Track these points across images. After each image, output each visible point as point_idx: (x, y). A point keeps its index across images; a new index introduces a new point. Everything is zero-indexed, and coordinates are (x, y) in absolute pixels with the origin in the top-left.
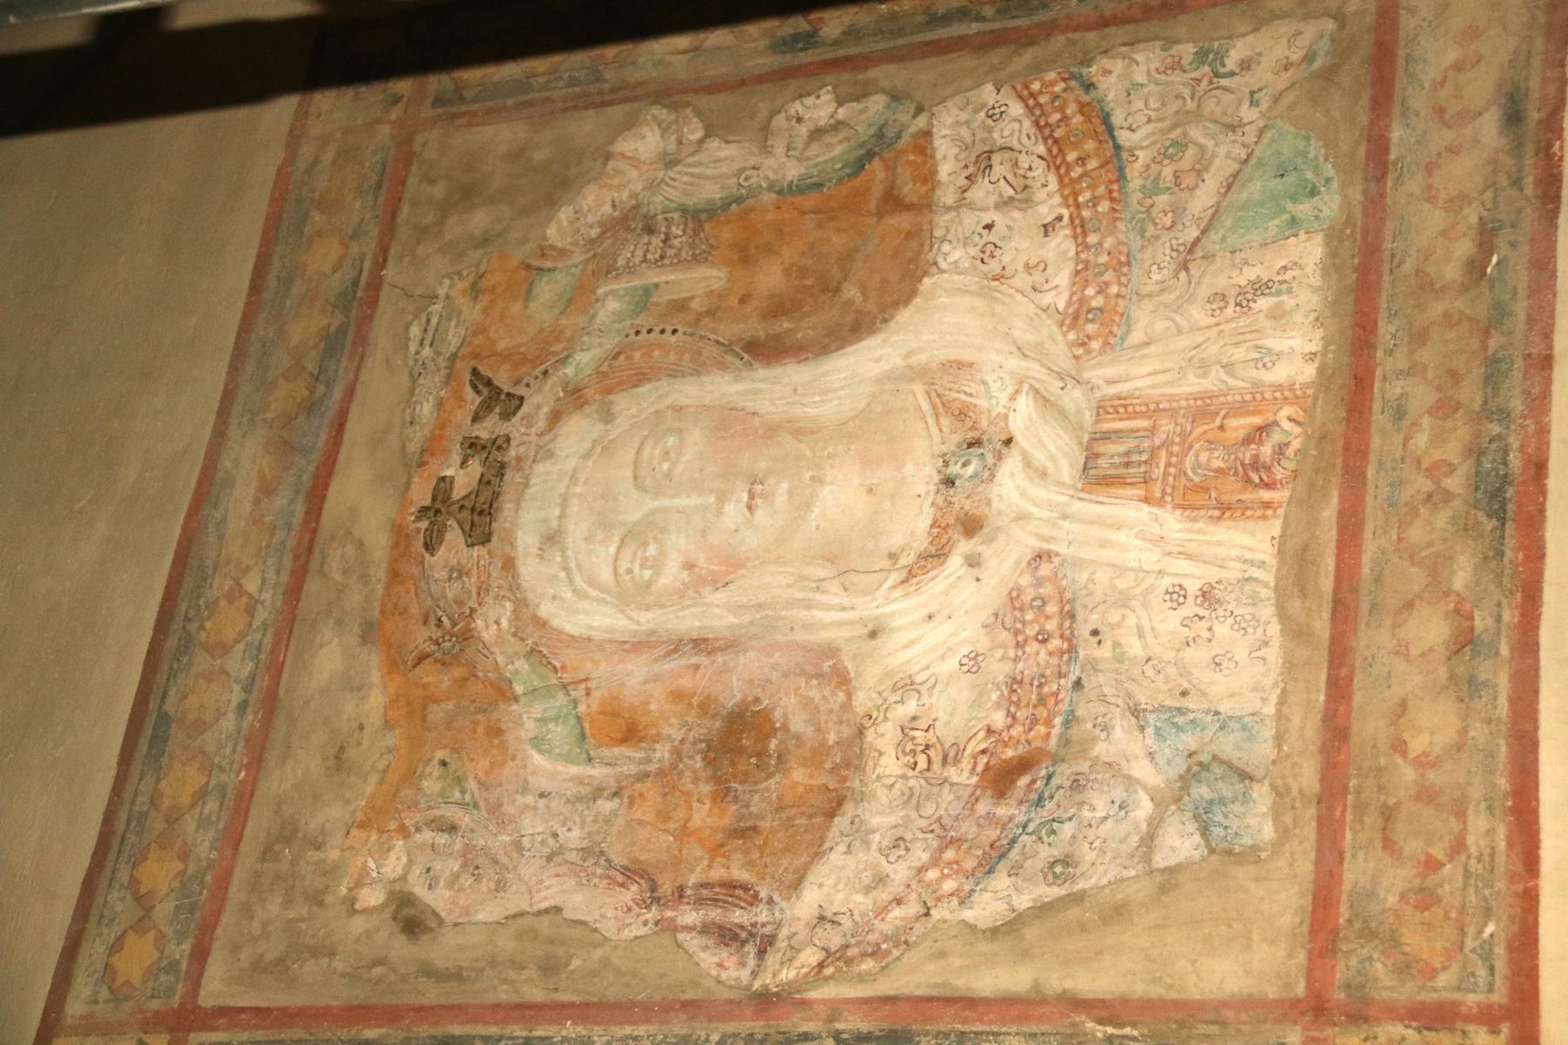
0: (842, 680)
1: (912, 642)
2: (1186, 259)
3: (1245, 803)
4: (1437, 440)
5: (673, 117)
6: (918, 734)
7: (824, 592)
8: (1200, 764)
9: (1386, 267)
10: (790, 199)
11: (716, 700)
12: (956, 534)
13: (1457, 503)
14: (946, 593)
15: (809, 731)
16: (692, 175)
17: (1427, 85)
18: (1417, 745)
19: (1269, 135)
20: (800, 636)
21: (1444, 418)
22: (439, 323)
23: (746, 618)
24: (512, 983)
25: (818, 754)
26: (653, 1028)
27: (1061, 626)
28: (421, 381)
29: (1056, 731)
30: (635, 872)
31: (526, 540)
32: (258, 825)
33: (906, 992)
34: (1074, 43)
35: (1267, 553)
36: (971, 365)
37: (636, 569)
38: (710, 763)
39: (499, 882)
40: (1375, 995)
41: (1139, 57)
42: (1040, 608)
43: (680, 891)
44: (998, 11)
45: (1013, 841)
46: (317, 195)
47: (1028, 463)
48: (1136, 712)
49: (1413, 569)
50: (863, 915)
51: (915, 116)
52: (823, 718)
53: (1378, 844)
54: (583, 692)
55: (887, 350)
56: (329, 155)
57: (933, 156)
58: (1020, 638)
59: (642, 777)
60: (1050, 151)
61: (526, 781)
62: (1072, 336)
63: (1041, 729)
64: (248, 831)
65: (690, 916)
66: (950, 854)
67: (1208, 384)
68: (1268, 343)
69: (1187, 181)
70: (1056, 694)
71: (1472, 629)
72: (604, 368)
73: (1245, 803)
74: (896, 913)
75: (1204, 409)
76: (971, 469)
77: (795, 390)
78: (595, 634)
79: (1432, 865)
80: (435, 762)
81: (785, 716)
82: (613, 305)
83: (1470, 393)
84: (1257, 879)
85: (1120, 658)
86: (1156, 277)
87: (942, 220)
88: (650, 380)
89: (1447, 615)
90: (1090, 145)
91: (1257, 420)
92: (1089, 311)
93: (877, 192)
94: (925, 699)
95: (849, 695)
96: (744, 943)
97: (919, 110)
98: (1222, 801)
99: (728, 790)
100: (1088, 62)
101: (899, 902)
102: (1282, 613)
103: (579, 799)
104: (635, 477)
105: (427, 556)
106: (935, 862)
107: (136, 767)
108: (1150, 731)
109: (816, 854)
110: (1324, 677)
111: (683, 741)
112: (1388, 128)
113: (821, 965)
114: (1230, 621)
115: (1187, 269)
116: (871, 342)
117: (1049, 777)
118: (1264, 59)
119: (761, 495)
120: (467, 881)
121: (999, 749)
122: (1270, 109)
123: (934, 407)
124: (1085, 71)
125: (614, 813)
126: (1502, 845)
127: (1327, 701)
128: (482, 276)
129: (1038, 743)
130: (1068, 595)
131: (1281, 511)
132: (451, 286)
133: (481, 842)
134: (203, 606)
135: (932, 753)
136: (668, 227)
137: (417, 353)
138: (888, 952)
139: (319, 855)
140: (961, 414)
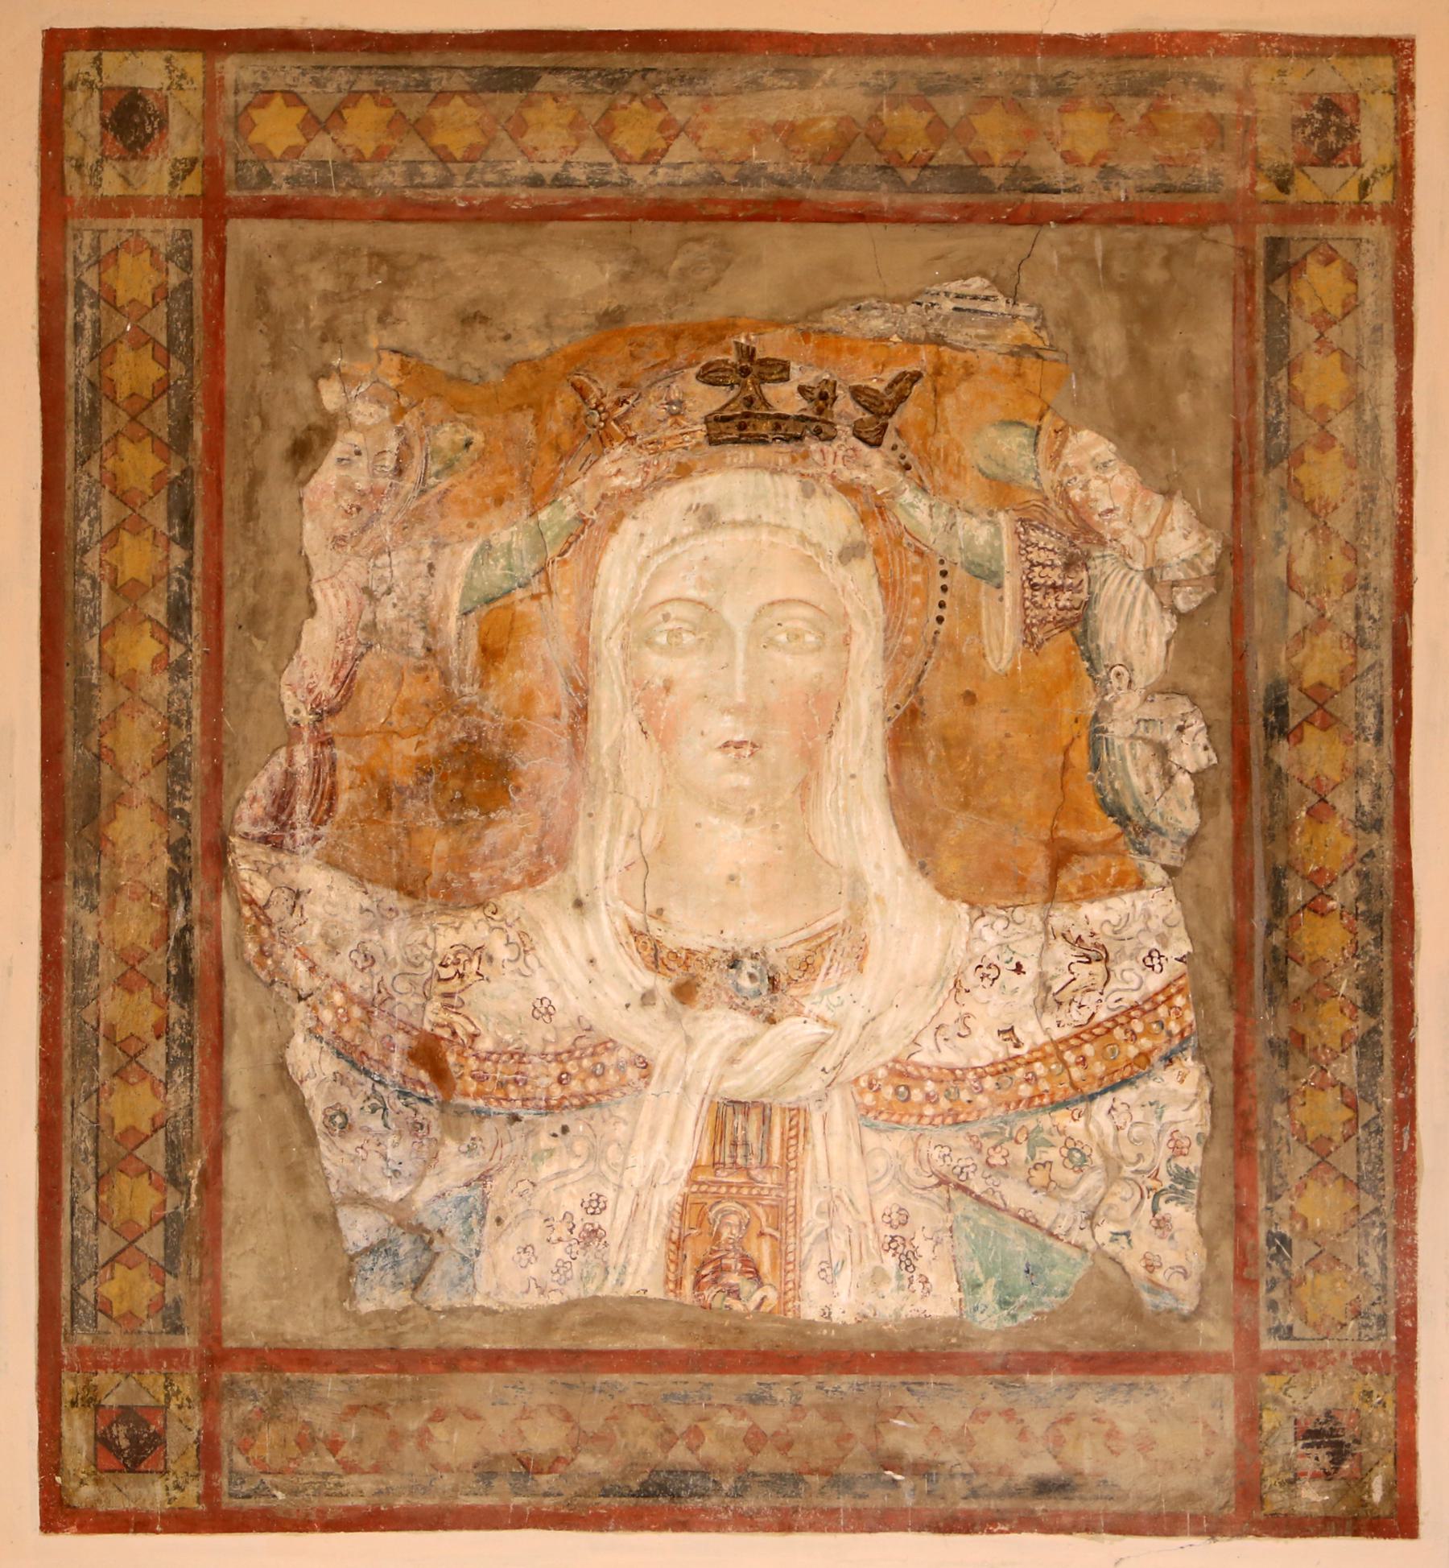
0: (533, 879)
1: (567, 946)
2: (951, 1183)
3: (394, 1285)
4: (725, 1438)
5: (1205, 572)
6: (475, 964)
7: (627, 844)
8: (431, 1242)
9: (910, 1378)
10: (1085, 733)
11: (523, 743)
12: (679, 976)
13: (659, 1456)
14: (617, 975)
15: (485, 849)
16: (1133, 604)
17: (1100, 1405)
18: (439, 1431)
19: (1075, 1254)
20: (582, 826)
21: (745, 1440)
22: (983, 313)
23: (606, 762)
24: (241, 579)
25: (461, 862)
26: (197, 740)
27: (573, 1095)
28: (911, 308)
29: (471, 1103)
30: (349, 688)
31: (711, 486)
32: (409, 237)
33: (228, 990)
34: (1223, 1039)
35: (632, 1286)
36: (861, 970)
37: (670, 625)
38: (457, 746)
39: (343, 538)
40: (226, 1405)
41: (1195, 1111)
42: (594, 1074)
43: (330, 742)
44: (1275, 949)
45: (367, 1073)
46: (1169, 101)
47: (746, 1043)
48: (484, 1177)
49: (601, 1421)
50: (300, 936)
51: (1164, 867)
52: (497, 863)
53: (353, 1402)
54: (536, 591)
55: (888, 873)
56: (1222, 105)
57: (1111, 894)
58: (564, 1056)
59: (445, 676)
60: (1098, 1025)
61: (445, 545)
62: (882, 1073)
63: (473, 1086)
64: (402, 226)
65: (302, 757)
66: (356, 1012)
67: (812, 1219)
68: (847, 1273)
69: (1039, 1177)
70: (507, 1099)
71: (540, 1472)
72: (906, 539)
73: (394, 1285)
74: (301, 968)
75: (784, 1215)
76: (745, 983)
77: (853, 776)
78: (598, 593)
79: (334, 1447)
80: (470, 433)
81: (501, 821)
82: (983, 534)
83: (768, 1461)
84: (325, 1300)
85: (539, 1157)
86: (936, 1153)
87: (1034, 917)
88: (885, 599)
89: (555, 1450)
90: (1099, 1068)
91: (765, 1268)
92: (907, 1088)
93: (1078, 835)
94: (509, 967)
95: (518, 887)
96: (276, 819)
97: (1171, 871)
98: (396, 1264)
99: (430, 773)
100: (1200, 1055)
101: (312, 969)
102: (571, 1305)
103: (426, 610)
104: (772, 604)
105: (696, 369)
106: (350, 999)
107: (480, 59)
108: (465, 1192)
109: (361, 878)
110: (508, 1346)
111: (481, 714)
112: (1061, 1371)
113: (252, 902)
114: (567, 1258)
115: (939, 1184)
116: (900, 856)
117: (426, 1101)
118: (1165, 1242)
119: (739, 756)
120: (347, 500)
121: (456, 1048)
122: (1105, 1255)
123: (819, 935)
124: (1189, 1054)
125: (409, 652)
126: (349, 1502)
127: (484, 1351)
128: (1038, 356)
129: (459, 1086)
130: (605, 1099)
131: (671, 1296)
132: (1027, 319)
133: (385, 508)
134: (658, 90)
135: (456, 981)
136: (1070, 588)
137: (947, 294)
138: (263, 966)
139: (372, 324)
140: (807, 966)
